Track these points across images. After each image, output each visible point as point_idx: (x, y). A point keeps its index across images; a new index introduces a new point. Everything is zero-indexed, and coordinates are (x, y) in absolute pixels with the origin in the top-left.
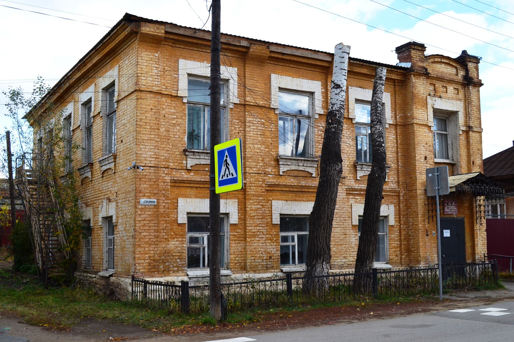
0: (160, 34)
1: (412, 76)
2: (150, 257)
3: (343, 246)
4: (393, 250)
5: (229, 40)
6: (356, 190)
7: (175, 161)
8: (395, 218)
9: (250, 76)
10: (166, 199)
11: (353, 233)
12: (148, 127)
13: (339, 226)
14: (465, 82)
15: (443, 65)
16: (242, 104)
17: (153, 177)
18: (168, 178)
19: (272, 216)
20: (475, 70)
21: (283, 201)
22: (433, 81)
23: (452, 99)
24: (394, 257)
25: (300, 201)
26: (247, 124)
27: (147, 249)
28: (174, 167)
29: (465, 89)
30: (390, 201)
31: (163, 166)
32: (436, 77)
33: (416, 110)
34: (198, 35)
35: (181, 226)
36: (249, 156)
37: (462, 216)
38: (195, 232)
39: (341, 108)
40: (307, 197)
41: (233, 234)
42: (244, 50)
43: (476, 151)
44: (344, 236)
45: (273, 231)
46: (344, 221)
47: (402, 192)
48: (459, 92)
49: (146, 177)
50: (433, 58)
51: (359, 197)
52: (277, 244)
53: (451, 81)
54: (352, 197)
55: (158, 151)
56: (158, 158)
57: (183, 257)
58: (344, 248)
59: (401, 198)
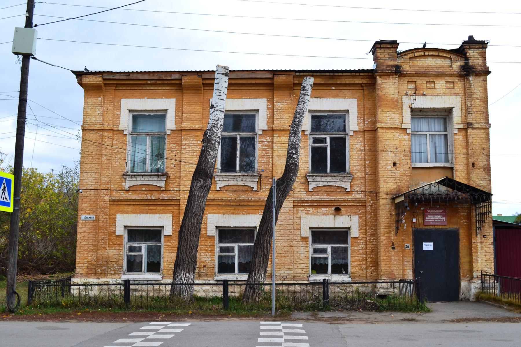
0: (98, 82)
1: (378, 77)
2: (88, 262)
3: (288, 257)
4: (356, 263)
5: (161, 76)
6: (307, 202)
7: (116, 184)
8: (359, 230)
9: (188, 104)
10: (105, 215)
11: (302, 245)
12: (90, 158)
13: (283, 238)
14: (462, 73)
15: (430, 59)
16: (179, 130)
17: (93, 198)
18: (107, 198)
19: (207, 228)
20: (479, 56)
21: (220, 215)
22: (413, 78)
23: (444, 94)
24: (358, 270)
25: (238, 214)
26: (183, 147)
27: (85, 255)
28: (115, 188)
29: (464, 81)
30: (353, 211)
31: (103, 189)
32: (415, 74)
33: (383, 113)
34: (132, 77)
35: (119, 237)
36: (184, 175)
37: (455, 227)
38: (320, 243)
39: (213, 127)
40: (247, 210)
41: (166, 244)
42: (178, 82)
43: (479, 151)
44: (290, 247)
45: (208, 242)
46: (289, 233)
47: (369, 202)
48: (455, 85)
49: (87, 198)
50: (412, 53)
51: (312, 209)
52: (212, 254)
53: (440, 75)
54: (302, 209)
55: (97, 176)
56: (97, 182)
57: (120, 263)
58: (288, 260)
59: (368, 208)
